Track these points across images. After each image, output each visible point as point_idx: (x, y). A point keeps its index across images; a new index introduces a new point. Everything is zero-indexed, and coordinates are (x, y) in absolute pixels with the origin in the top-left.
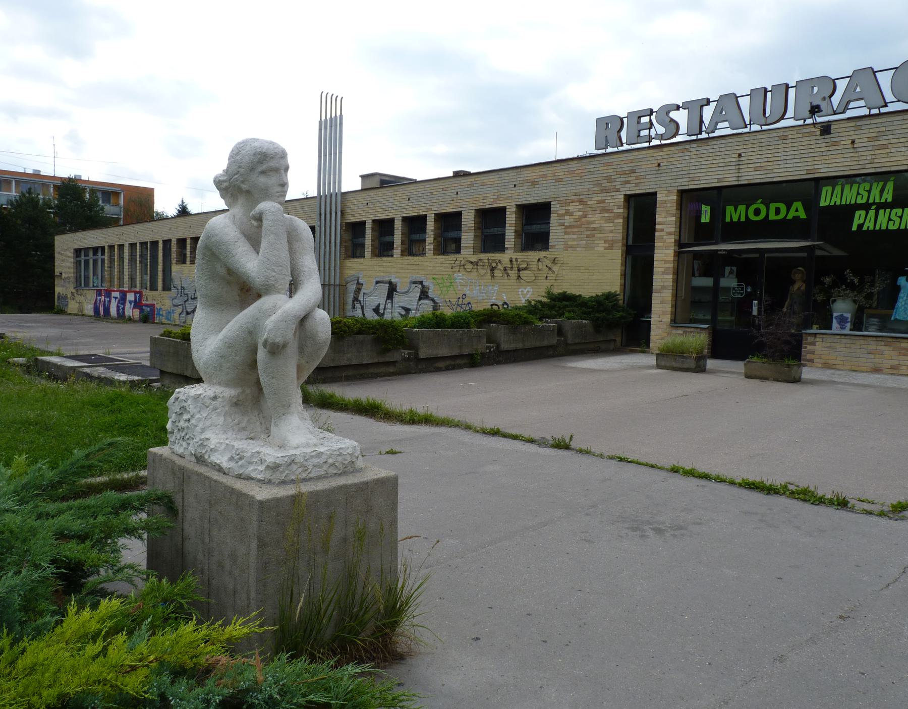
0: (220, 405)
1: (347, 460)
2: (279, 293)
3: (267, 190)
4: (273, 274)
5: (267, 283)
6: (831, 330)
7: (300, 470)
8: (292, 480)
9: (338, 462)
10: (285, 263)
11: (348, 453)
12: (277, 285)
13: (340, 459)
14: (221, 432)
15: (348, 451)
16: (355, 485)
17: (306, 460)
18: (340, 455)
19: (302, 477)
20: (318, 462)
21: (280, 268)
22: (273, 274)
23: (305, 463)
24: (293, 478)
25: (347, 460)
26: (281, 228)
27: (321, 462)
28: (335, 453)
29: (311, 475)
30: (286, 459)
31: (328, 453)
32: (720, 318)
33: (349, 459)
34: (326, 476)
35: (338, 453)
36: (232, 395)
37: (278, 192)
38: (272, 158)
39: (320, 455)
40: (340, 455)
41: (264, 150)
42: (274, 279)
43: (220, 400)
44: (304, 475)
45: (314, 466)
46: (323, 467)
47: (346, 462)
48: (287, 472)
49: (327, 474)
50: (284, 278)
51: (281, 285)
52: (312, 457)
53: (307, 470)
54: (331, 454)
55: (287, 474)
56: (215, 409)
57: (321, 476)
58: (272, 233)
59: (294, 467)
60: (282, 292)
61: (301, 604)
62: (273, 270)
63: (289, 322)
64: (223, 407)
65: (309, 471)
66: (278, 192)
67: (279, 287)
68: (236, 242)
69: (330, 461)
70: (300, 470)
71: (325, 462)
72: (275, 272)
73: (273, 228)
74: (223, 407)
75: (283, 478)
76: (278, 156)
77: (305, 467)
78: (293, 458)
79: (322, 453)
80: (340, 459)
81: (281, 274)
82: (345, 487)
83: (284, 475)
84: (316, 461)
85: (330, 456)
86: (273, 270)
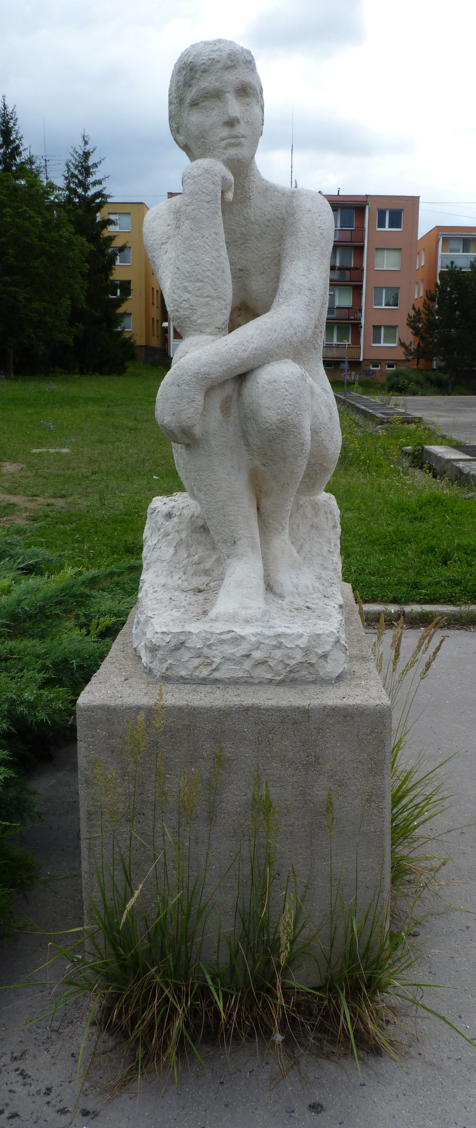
0: (174, 527)
1: (294, 658)
2: (202, 332)
3: (203, 137)
4: (186, 296)
5: (177, 314)
6: (385, 227)
7: (196, 662)
8: (182, 677)
9: (273, 659)
10: (209, 274)
11: (298, 646)
12: (194, 318)
13: (278, 654)
14: (165, 574)
15: (299, 642)
16: (279, 709)
17: (209, 646)
18: (280, 646)
19: (202, 675)
20: (233, 654)
21: (199, 284)
22: (186, 296)
23: (206, 651)
24: (183, 673)
25: (294, 658)
26: (206, 205)
27: (238, 655)
28: (267, 641)
29: (217, 675)
30: (168, 639)
31: (254, 639)
32: (352, 266)
33: (299, 657)
34: (251, 680)
35: (275, 643)
36: (196, 514)
37: (223, 139)
38: (204, 71)
39: (238, 640)
40: (279, 646)
41: (191, 59)
42: (187, 306)
43: (175, 520)
44: (204, 672)
45: (226, 659)
46: (241, 664)
47: (293, 662)
48: (170, 661)
49: (252, 677)
50: (207, 304)
51: (202, 316)
52: (223, 642)
53: (210, 664)
54: (261, 643)
55: (171, 664)
56: (167, 534)
57: (238, 679)
58: (187, 218)
59: (186, 656)
60: (208, 330)
61: (132, 901)
62: (185, 289)
63: (184, 387)
64: (178, 531)
65: (214, 666)
66: (223, 139)
67: (200, 321)
68: (163, 244)
69: (257, 655)
70: (196, 662)
71: (248, 656)
72: (188, 292)
73: (189, 209)
74: (178, 531)
75: (163, 671)
76: (219, 65)
77: (208, 658)
78: (183, 638)
79: (243, 638)
80: (278, 654)
81: (201, 296)
82: (257, 710)
83: (165, 665)
84: (229, 650)
85: (258, 646)
86: (185, 289)
